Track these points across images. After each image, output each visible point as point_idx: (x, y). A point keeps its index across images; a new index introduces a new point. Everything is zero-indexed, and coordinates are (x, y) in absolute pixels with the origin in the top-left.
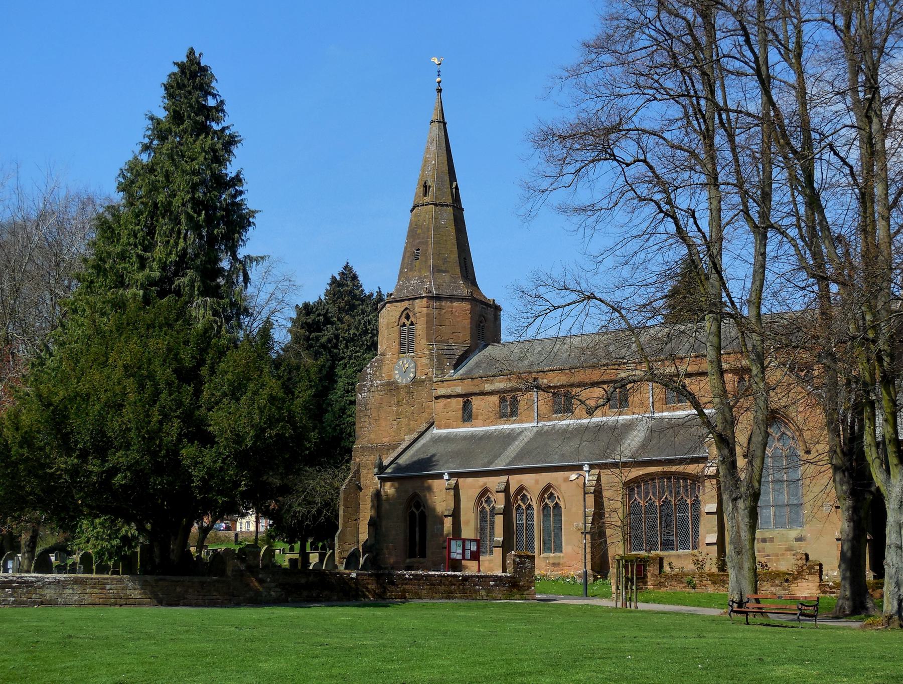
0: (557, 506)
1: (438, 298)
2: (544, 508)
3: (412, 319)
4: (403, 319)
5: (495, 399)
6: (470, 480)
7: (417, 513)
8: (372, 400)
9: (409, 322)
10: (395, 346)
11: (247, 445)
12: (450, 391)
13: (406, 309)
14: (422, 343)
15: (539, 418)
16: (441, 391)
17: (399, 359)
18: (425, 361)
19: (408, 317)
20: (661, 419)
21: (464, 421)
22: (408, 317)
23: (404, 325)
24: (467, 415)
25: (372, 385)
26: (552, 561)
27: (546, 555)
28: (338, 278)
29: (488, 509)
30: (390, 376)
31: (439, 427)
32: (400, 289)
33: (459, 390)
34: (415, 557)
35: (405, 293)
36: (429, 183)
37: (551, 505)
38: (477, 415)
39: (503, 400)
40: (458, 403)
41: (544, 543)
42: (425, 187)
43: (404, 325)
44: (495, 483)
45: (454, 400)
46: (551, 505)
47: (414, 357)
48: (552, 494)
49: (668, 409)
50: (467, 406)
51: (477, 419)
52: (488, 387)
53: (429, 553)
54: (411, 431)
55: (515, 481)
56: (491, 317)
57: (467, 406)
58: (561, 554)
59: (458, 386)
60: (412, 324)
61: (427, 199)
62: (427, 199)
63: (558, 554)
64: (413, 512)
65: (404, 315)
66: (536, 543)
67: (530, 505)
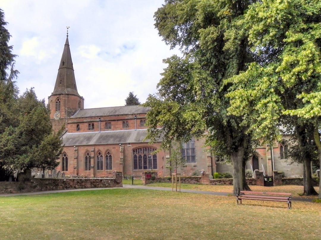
0: (110, 156)
1: (68, 94)
2: (106, 157)
5: (87, 124)
6: (82, 148)
10: (54, 109)
11: (214, 131)
14: (62, 108)
15: (101, 130)
16: (70, 122)
17: (55, 112)
18: (63, 113)
19: (58, 100)
20: (102, 133)
21: (77, 131)
22: (58, 100)
24: (78, 129)
26: (109, 172)
27: (107, 170)
30: (52, 117)
31: (69, 132)
33: (76, 121)
35: (58, 93)
36: (64, 62)
37: (109, 156)
39: (90, 125)
40: (76, 125)
41: (106, 167)
43: (57, 102)
44: (91, 149)
46: (109, 156)
47: (60, 112)
48: (109, 152)
49: (141, 128)
50: (78, 126)
51: (81, 130)
52: (85, 121)
55: (97, 149)
56: (81, 102)
57: (78, 126)
60: (60, 102)
61: (64, 66)
62: (64, 66)
63: (110, 170)
65: (57, 99)
67: (102, 156)
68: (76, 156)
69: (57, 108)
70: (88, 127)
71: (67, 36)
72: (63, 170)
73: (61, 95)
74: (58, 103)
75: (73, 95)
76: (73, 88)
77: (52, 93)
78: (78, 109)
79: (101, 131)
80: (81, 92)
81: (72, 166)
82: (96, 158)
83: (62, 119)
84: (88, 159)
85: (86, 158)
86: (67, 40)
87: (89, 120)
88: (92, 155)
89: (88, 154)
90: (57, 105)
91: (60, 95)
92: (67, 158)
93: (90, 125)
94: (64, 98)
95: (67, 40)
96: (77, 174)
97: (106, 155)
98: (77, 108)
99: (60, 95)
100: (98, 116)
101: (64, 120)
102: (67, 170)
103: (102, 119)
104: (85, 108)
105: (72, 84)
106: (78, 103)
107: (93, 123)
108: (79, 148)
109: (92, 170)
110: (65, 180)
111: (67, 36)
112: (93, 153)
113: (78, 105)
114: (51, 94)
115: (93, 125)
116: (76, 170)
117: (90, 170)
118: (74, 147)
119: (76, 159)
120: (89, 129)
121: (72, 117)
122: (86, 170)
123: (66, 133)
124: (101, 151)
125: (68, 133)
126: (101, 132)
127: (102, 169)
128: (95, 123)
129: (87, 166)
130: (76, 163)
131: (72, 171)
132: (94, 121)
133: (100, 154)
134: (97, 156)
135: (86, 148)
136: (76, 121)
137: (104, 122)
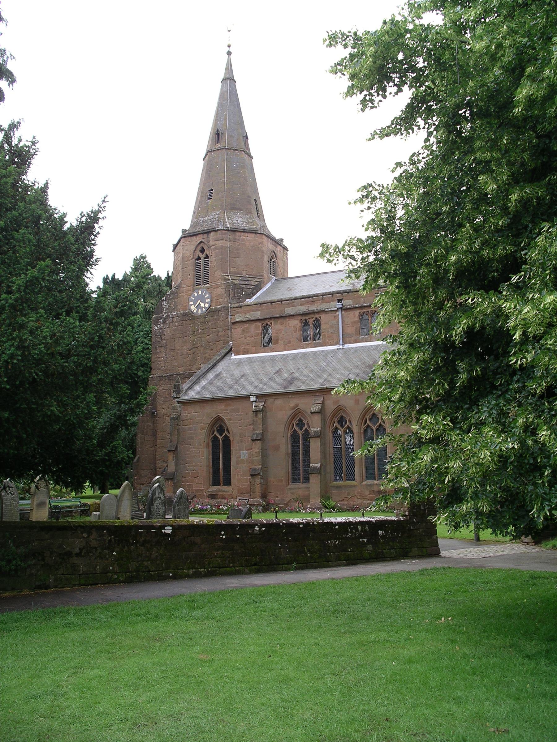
1: (233, 231)
2: (365, 431)
3: (207, 252)
4: (198, 253)
5: (296, 323)
6: (279, 402)
7: (220, 438)
8: (167, 332)
9: (204, 255)
12: (248, 316)
13: (201, 242)
16: (238, 318)
17: (194, 290)
18: (220, 291)
19: (202, 251)
22: (202, 251)
23: (199, 258)
24: (268, 343)
25: (167, 317)
27: (369, 482)
28: (133, 267)
29: (300, 433)
31: (237, 353)
32: (193, 225)
33: (258, 314)
34: (219, 484)
35: (198, 229)
38: (278, 340)
39: (306, 324)
42: (218, 134)
43: (199, 258)
45: (254, 324)
47: (208, 288)
52: (289, 311)
53: (234, 480)
54: (207, 360)
58: (353, 483)
59: (257, 310)
60: (207, 257)
61: (219, 145)
64: (215, 437)
65: (199, 248)
66: (356, 469)
68: (259, 431)
69: (198, 277)
70: (299, 334)
71: (229, 53)
72: (216, 482)
73: (212, 234)
74: (202, 261)
75: (250, 231)
76: (249, 212)
77: (184, 231)
78: (269, 279)
79: (344, 343)
80: (275, 223)
81: (245, 467)
82: (330, 436)
83: (217, 311)
84: (299, 441)
85: (295, 437)
86: (229, 67)
87: (303, 309)
88: (315, 428)
89: (301, 424)
90: (198, 265)
91: (208, 232)
92: (227, 442)
93: (306, 324)
94: (219, 243)
95: (229, 67)
96: (264, 496)
97: (363, 427)
98: (265, 275)
99: (208, 232)
100: (333, 293)
101: (222, 314)
102: (228, 482)
103: (348, 302)
104: (291, 273)
105: (250, 203)
106: (266, 258)
107: (317, 316)
108: (269, 401)
109: (315, 480)
110: (168, 530)
111: (229, 53)
112: (317, 419)
113: (266, 265)
114: (180, 235)
115: (318, 324)
116: (258, 480)
117: (307, 480)
118: (252, 399)
119: (258, 444)
120: (305, 339)
121: (249, 301)
122: (295, 480)
123: (228, 357)
124: (345, 411)
125: (234, 357)
126: (346, 346)
127: (351, 476)
128: (324, 318)
129: (300, 471)
130: (260, 458)
131: (245, 485)
132: (319, 312)
133: (342, 421)
134: (331, 429)
135: (293, 402)
136: (259, 313)
137: (357, 312)
